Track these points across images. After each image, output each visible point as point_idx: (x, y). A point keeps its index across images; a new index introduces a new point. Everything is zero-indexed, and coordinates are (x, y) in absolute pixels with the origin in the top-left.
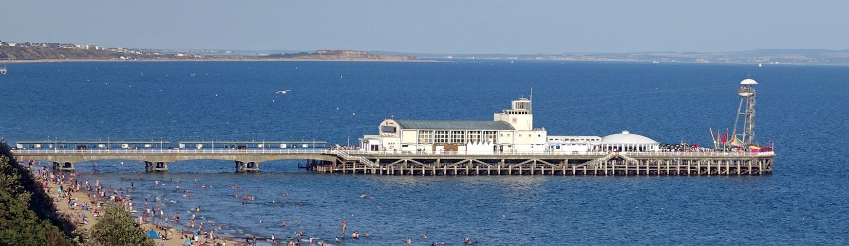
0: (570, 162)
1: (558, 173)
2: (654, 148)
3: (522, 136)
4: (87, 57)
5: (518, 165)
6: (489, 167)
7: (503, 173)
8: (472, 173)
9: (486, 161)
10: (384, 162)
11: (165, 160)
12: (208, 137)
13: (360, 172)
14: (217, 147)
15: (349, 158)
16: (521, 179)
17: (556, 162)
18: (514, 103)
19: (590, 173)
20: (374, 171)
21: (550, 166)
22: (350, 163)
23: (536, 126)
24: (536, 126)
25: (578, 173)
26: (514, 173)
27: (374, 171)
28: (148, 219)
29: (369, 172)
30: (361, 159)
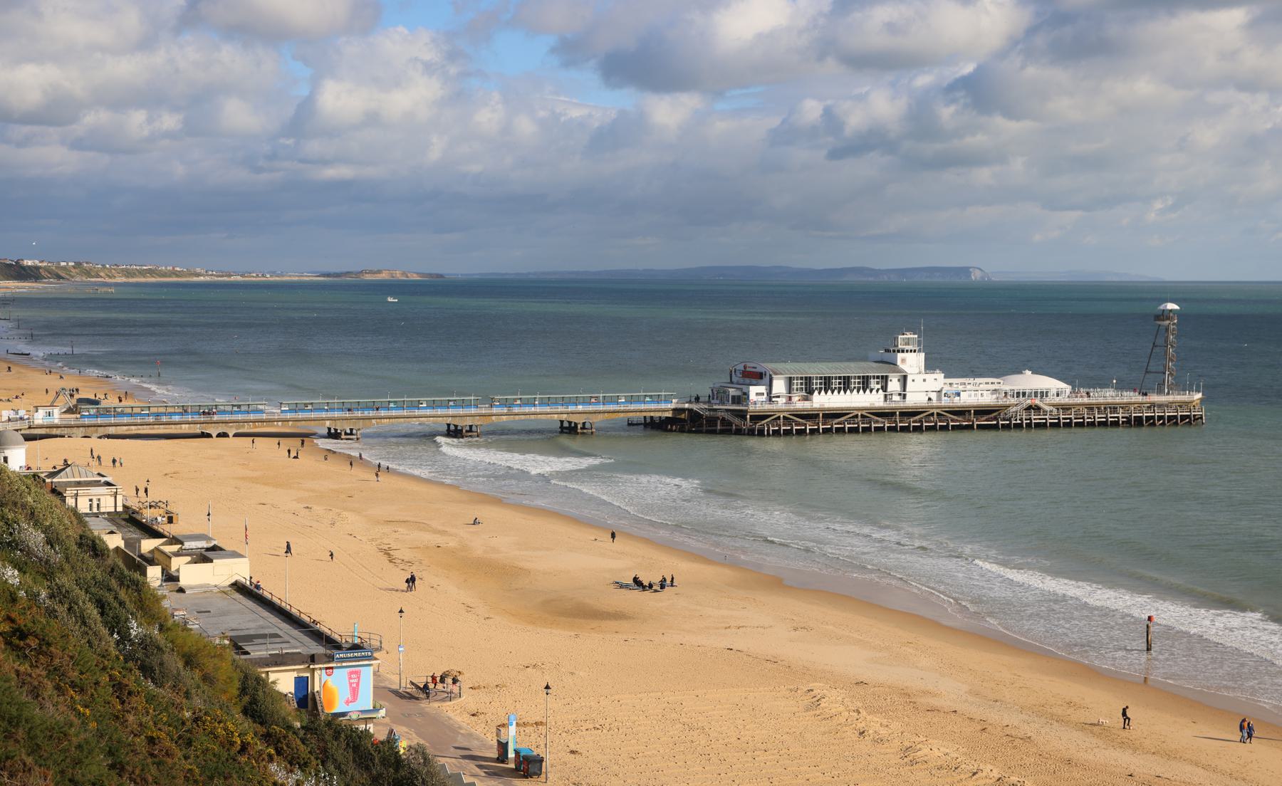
0: (902, 414)
23: (930, 366)
24: (930, 366)
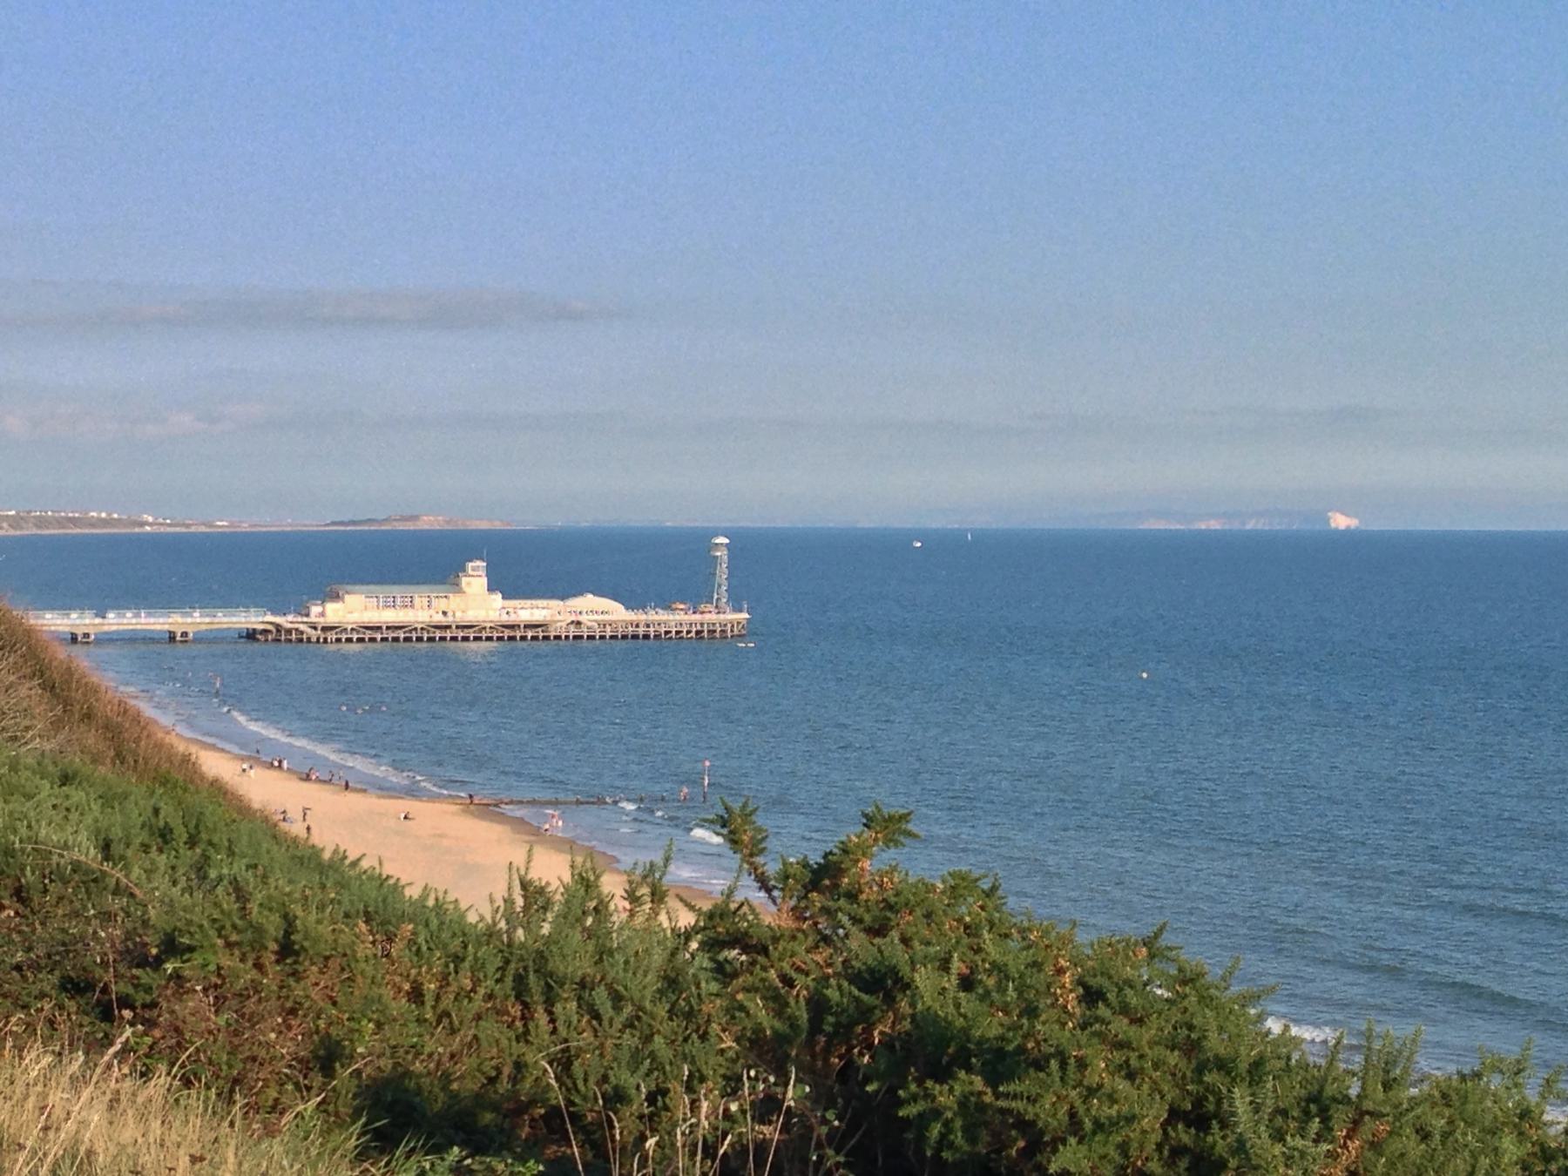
1: (511, 638)
2: (615, 613)
3: (476, 601)
4: (114, 527)
5: (470, 632)
6: (438, 634)
7: (454, 639)
8: (419, 639)
9: (436, 627)
10: (325, 629)
11: (91, 631)
12: (137, 607)
13: (301, 640)
14: (1435, 973)
15: (289, 626)
16: (473, 645)
17: (512, 627)
18: (470, 565)
19: (546, 638)
20: (314, 639)
21: (509, 633)
22: (289, 631)
23: (491, 589)
24: (491, 589)
25: (533, 638)
26: (465, 639)
27: (314, 639)
28: (481, 976)
29: (309, 640)
30: (302, 627)
